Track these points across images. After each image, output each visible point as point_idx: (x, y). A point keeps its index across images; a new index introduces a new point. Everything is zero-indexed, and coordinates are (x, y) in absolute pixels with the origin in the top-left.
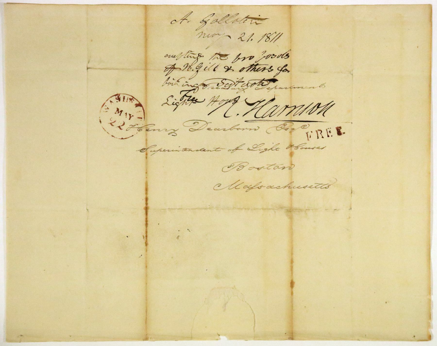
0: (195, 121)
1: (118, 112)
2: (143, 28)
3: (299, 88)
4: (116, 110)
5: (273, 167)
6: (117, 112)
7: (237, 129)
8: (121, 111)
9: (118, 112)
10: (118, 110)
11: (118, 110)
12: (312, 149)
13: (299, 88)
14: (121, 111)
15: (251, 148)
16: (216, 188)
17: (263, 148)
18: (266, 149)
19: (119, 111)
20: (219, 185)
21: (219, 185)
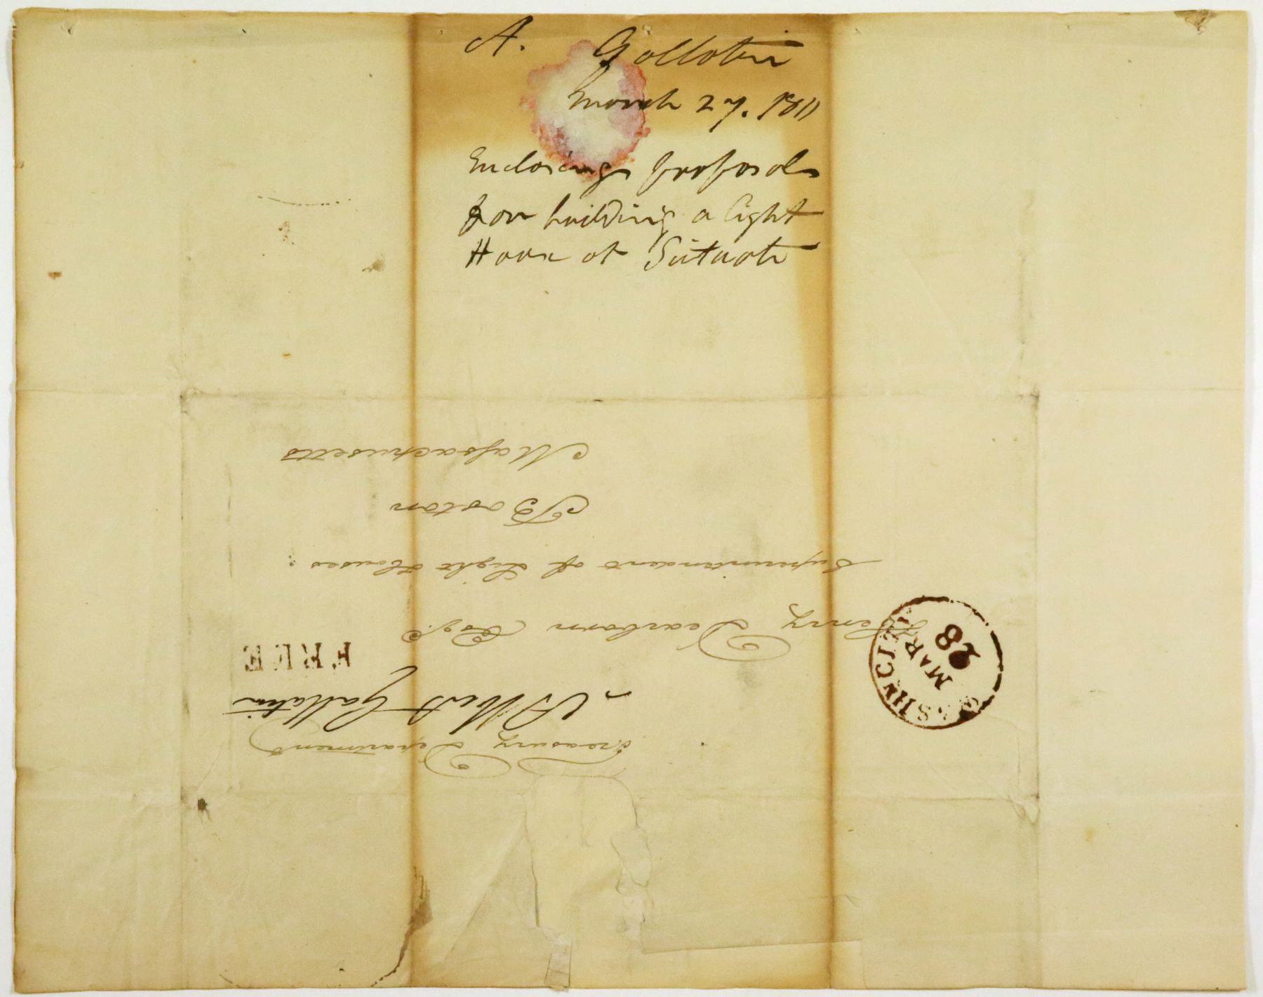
0: (859, 692)
1: (941, 675)
2: (843, 927)
3: (591, 628)
4: (942, 687)
5: (439, 509)
6: (944, 678)
7: (614, 627)
8: (931, 675)
9: (941, 675)
10: (938, 685)
11: (938, 685)
12: (349, 564)
13: (591, 628)
14: (931, 675)
15: (517, 569)
16: (582, 449)
17: (489, 569)
18: (481, 565)
19: (935, 679)
20: (577, 456)
21: (577, 456)
